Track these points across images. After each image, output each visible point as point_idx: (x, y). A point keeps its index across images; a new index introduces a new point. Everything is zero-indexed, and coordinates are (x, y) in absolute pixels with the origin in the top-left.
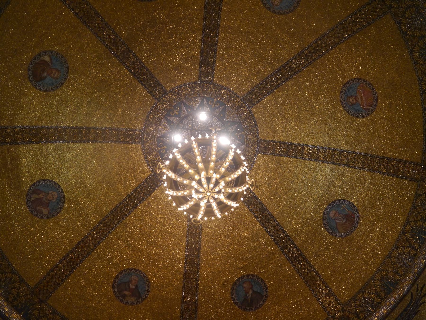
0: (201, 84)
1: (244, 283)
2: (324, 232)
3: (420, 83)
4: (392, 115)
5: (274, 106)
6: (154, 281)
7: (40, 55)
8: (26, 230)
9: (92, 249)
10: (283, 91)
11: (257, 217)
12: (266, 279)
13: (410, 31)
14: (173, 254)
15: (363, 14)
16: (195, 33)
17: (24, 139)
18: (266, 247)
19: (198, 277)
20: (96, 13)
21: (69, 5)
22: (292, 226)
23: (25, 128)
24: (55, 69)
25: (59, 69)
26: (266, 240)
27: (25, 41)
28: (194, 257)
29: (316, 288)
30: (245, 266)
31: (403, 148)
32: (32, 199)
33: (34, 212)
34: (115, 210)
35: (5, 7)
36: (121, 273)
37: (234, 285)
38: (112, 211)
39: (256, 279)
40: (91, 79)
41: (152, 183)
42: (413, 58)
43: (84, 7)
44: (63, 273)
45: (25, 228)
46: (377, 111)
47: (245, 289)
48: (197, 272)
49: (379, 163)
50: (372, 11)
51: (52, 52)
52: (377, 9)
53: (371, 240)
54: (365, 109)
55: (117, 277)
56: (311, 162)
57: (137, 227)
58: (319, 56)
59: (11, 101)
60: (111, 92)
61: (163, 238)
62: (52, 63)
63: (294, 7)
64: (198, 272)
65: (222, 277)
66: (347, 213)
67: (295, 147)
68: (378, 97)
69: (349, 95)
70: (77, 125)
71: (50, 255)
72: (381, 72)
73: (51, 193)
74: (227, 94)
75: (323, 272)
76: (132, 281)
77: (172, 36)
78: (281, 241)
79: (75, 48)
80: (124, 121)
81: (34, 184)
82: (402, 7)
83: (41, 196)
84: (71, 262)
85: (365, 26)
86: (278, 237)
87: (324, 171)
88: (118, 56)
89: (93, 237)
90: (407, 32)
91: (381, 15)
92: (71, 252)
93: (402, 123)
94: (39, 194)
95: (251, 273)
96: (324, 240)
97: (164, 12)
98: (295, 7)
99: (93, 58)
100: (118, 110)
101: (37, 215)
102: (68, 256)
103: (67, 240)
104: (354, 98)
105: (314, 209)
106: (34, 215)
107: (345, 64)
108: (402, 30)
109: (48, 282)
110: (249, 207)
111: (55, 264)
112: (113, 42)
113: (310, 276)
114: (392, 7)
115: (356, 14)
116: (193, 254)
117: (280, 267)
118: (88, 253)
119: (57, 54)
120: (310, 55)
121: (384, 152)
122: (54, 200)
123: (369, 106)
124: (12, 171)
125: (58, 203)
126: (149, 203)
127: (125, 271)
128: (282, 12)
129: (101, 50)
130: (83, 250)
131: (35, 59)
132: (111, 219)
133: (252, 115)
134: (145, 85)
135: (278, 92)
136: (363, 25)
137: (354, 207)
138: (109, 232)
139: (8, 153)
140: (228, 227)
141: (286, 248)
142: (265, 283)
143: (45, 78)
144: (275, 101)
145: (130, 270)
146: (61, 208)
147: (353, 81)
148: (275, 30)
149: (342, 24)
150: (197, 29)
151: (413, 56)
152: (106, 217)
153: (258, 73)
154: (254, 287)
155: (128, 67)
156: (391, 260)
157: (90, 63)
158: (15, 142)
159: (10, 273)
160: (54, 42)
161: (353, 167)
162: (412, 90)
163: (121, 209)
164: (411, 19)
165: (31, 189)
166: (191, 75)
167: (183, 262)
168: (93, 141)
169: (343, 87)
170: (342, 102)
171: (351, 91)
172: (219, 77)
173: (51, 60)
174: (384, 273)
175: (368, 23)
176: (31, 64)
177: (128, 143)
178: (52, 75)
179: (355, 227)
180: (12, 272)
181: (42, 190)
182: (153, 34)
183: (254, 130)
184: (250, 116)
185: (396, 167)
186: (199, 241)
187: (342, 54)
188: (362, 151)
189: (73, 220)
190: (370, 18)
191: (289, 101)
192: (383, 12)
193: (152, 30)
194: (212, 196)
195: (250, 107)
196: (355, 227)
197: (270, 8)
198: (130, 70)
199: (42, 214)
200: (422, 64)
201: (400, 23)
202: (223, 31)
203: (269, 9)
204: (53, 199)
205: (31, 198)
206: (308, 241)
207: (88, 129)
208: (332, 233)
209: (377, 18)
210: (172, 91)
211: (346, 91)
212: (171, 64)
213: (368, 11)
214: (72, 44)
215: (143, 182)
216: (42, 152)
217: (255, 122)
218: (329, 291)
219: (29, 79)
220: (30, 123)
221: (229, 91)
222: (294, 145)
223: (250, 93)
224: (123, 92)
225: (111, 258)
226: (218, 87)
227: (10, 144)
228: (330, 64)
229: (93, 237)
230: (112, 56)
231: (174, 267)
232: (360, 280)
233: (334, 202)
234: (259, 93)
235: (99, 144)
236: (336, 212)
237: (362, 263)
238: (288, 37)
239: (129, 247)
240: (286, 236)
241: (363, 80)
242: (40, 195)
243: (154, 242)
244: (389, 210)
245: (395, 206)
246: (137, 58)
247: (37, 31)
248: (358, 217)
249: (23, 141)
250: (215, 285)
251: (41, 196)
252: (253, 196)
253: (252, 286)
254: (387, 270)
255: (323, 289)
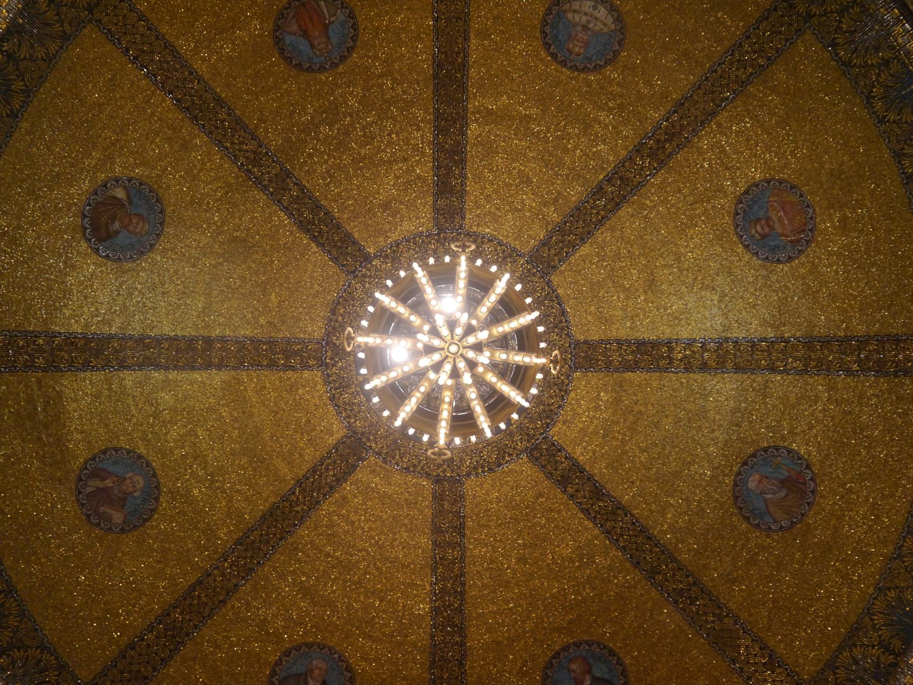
0: (438, 234)
1: (570, 661)
2: (741, 525)
3: (899, 162)
4: (852, 243)
5: (597, 267)
6: (363, 670)
7: (105, 186)
8: (74, 556)
9: (220, 602)
10: (613, 230)
11: (586, 511)
12: (620, 648)
13: (857, 58)
14: (404, 607)
15: (755, 43)
16: (418, 130)
17: (73, 362)
18: (614, 576)
19: (464, 656)
20: (219, 101)
21: (163, 84)
22: (665, 527)
23: (75, 337)
24: (136, 215)
25: (145, 216)
26: (613, 560)
27: (76, 156)
28: (451, 610)
29: (739, 653)
30: (569, 622)
31: (889, 310)
32: (89, 490)
33: (92, 518)
34: (271, 515)
35: (36, 87)
36: (287, 653)
37: (548, 668)
38: (263, 517)
39: (598, 650)
40: (211, 237)
41: (349, 454)
42: (874, 113)
43: (193, 88)
44: (156, 654)
45: (73, 551)
46: (818, 242)
47: (573, 675)
48: (461, 646)
49: (841, 353)
50: (772, 33)
51: (130, 181)
52: (782, 26)
53: (850, 526)
54: (791, 241)
55: (279, 663)
56: (691, 375)
57: (321, 552)
58: (678, 146)
59: (48, 280)
60: (254, 262)
61: (381, 573)
62: (130, 203)
63: (614, 52)
64: (462, 644)
65: (518, 651)
66: (786, 474)
67: (652, 347)
68: (814, 210)
69: (752, 218)
70: (186, 334)
71: (128, 613)
72: (813, 157)
73: (130, 478)
74: (496, 250)
75: (751, 615)
76: (312, 671)
77: (373, 139)
78: (645, 558)
79: (177, 172)
80: (284, 322)
81: (93, 458)
82: (832, 12)
83: (108, 483)
84: (174, 629)
85: (763, 66)
86: (637, 550)
87: (723, 389)
88: (265, 186)
89: (223, 575)
90: (851, 61)
91: (792, 38)
92: (174, 607)
93: (875, 257)
94: (104, 480)
95: (586, 637)
96: (742, 545)
97: (353, 91)
98: (616, 53)
99: (215, 192)
100: (270, 299)
101: (99, 525)
102: (168, 615)
103: (165, 580)
104: (763, 222)
105: (712, 477)
106: (93, 524)
107: (734, 154)
108: (840, 58)
109: (122, 673)
110: (565, 490)
111: (138, 633)
112: (255, 158)
113: (722, 630)
114: (810, 16)
115: (740, 45)
116: (450, 606)
117: (651, 617)
118: (212, 610)
119: (141, 184)
120: (659, 149)
121: (847, 328)
122: (137, 494)
123: (799, 233)
124: (46, 426)
125: (145, 500)
126: (344, 498)
127: (298, 648)
128: (591, 67)
129: (230, 174)
130: (202, 601)
131: (96, 194)
132: (261, 535)
133: (553, 291)
134: (323, 244)
135: (603, 235)
136: (760, 66)
137: (799, 459)
138: (259, 563)
139: (40, 389)
140: (524, 539)
141: (659, 573)
142: (619, 657)
143: (117, 233)
144: (598, 255)
145: (307, 646)
146: (152, 510)
147: (757, 186)
148: (581, 106)
149: (716, 71)
150: (422, 121)
151: (873, 107)
152: (251, 530)
153: (556, 200)
154: (594, 669)
155: (287, 208)
156: (904, 562)
157: (208, 203)
158: (55, 367)
159: (37, 648)
160: (135, 159)
161: (786, 372)
162: (885, 181)
163: (284, 513)
164: (854, 31)
165: (86, 468)
166: (418, 218)
167: (426, 625)
168: (219, 367)
169: (738, 204)
170: (741, 237)
171: (755, 208)
172: (523, 470)
173: (129, 197)
174: (892, 594)
175: (769, 58)
176: (89, 205)
177: (293, 368)
178: (132, 228)
179: (808, 504)
180: (43, 648)
181: (110, 470)
182: (334, 139)
183: (561, 322)
184: (549, 293)
185: (878, 353)
186: (461, 575)
187: (726, 135)
188: (798, 334)
189: (178, 536)
190: (771, 48)
191: (629, 252)
192: (796, 31)
193: (330, 130)
194: (462, 355)
195: (546, 274)
196: (808, 504)
197: (564, 61)
198: (290, 215)
199: (110, 522)
200: (894, 122)
201: (834, 45)
202: (476, 120)
203: (563, 63)
204: (135, 491)
205: (86, 486)
206: (707, 551)
207: (208, 341)
208: (758, 525)
209: (785, 46)
210: (382, 255)
211: (745, 211)
212: (374, 198)
213: (764, 34)
214: (171, 164)
215: (330, 452)
216: (110, 389)
217: (560, 305)
218: (770, 657)
219: (84, 234)
220: (87, 326)
221: (500, 244)
222: (651, 343)
223: (544, 245)
224: (279, 261)
225: (265, 620)
226: (475, 237)
227: (45, 370)
228: (704, 159)
229: (223, 575)
230: (251, 186)
231: (406, 636)
232: (838, 621)
233: (754, 455)
234: (563, 242)
235: (233, 373)
236: (762, 476)
237: (837, 582)
238: (608, 117)
239: (304, 596)
240: (656, 546)
241: (778, 180)
242: (107, 481)
243: (360, 583)
244: (881, 452)
245: (892, 440)
246: (303, 190)
247: (100, 136)
248: (812, 479)
249: (70, 366)
250: (504, 671)
251: (108, 483)
252: (574, 465)
253: (590, 665)
254: (897, 587)
255: (755, 655)
